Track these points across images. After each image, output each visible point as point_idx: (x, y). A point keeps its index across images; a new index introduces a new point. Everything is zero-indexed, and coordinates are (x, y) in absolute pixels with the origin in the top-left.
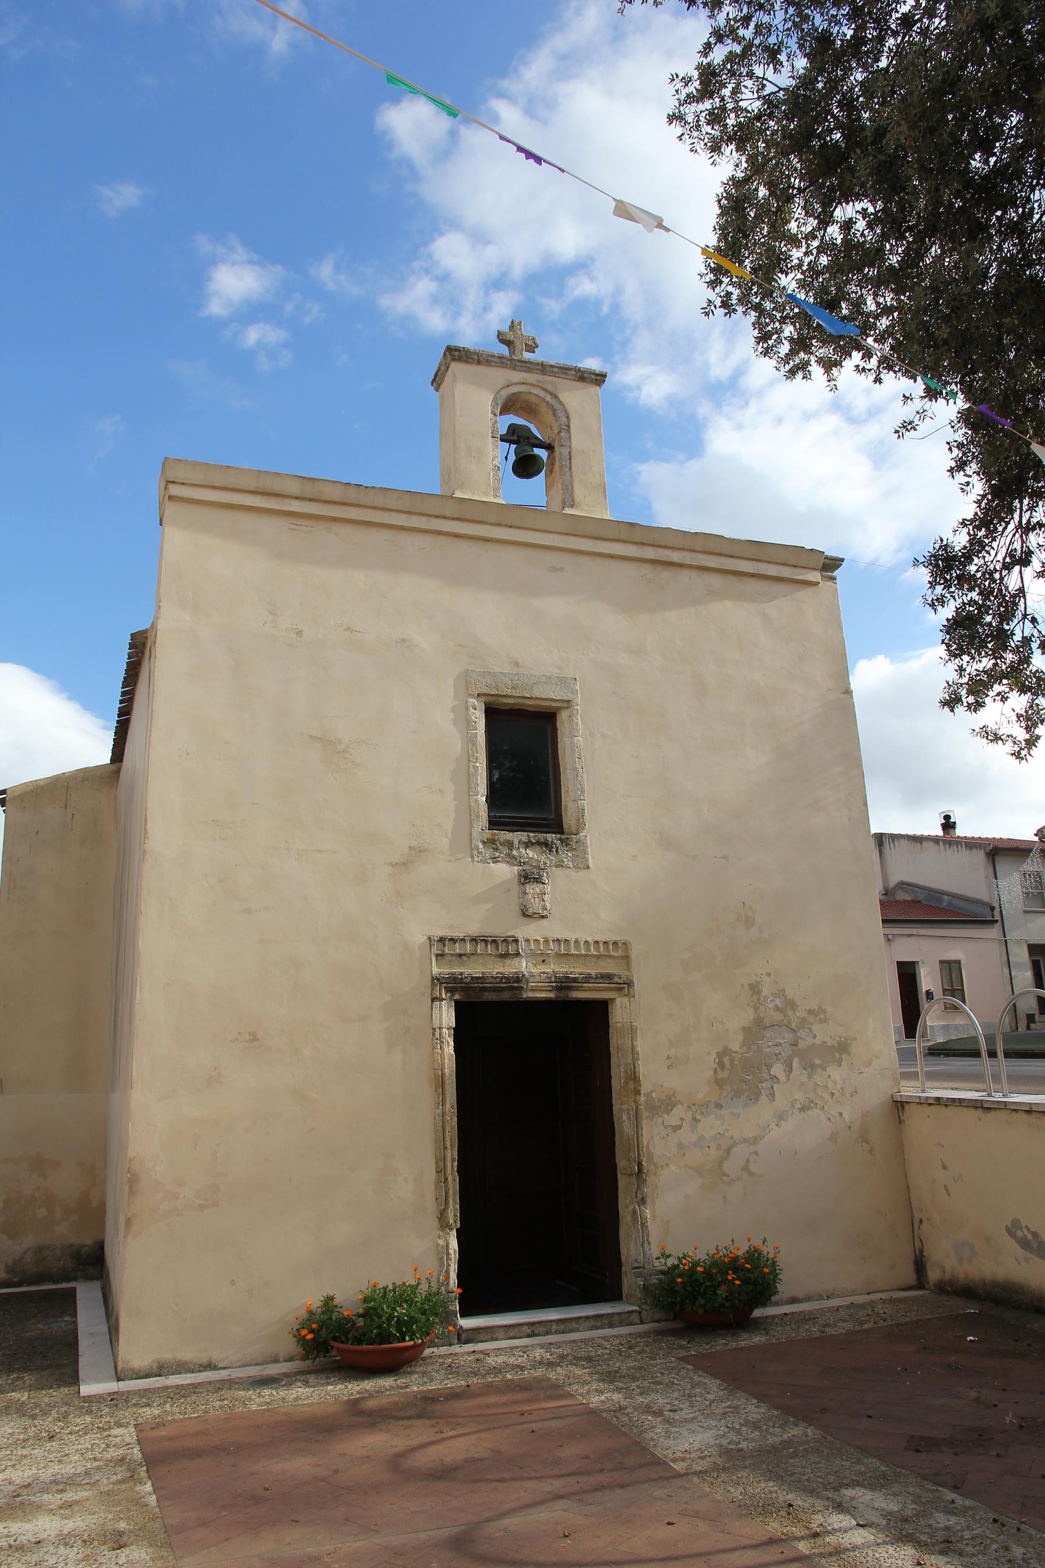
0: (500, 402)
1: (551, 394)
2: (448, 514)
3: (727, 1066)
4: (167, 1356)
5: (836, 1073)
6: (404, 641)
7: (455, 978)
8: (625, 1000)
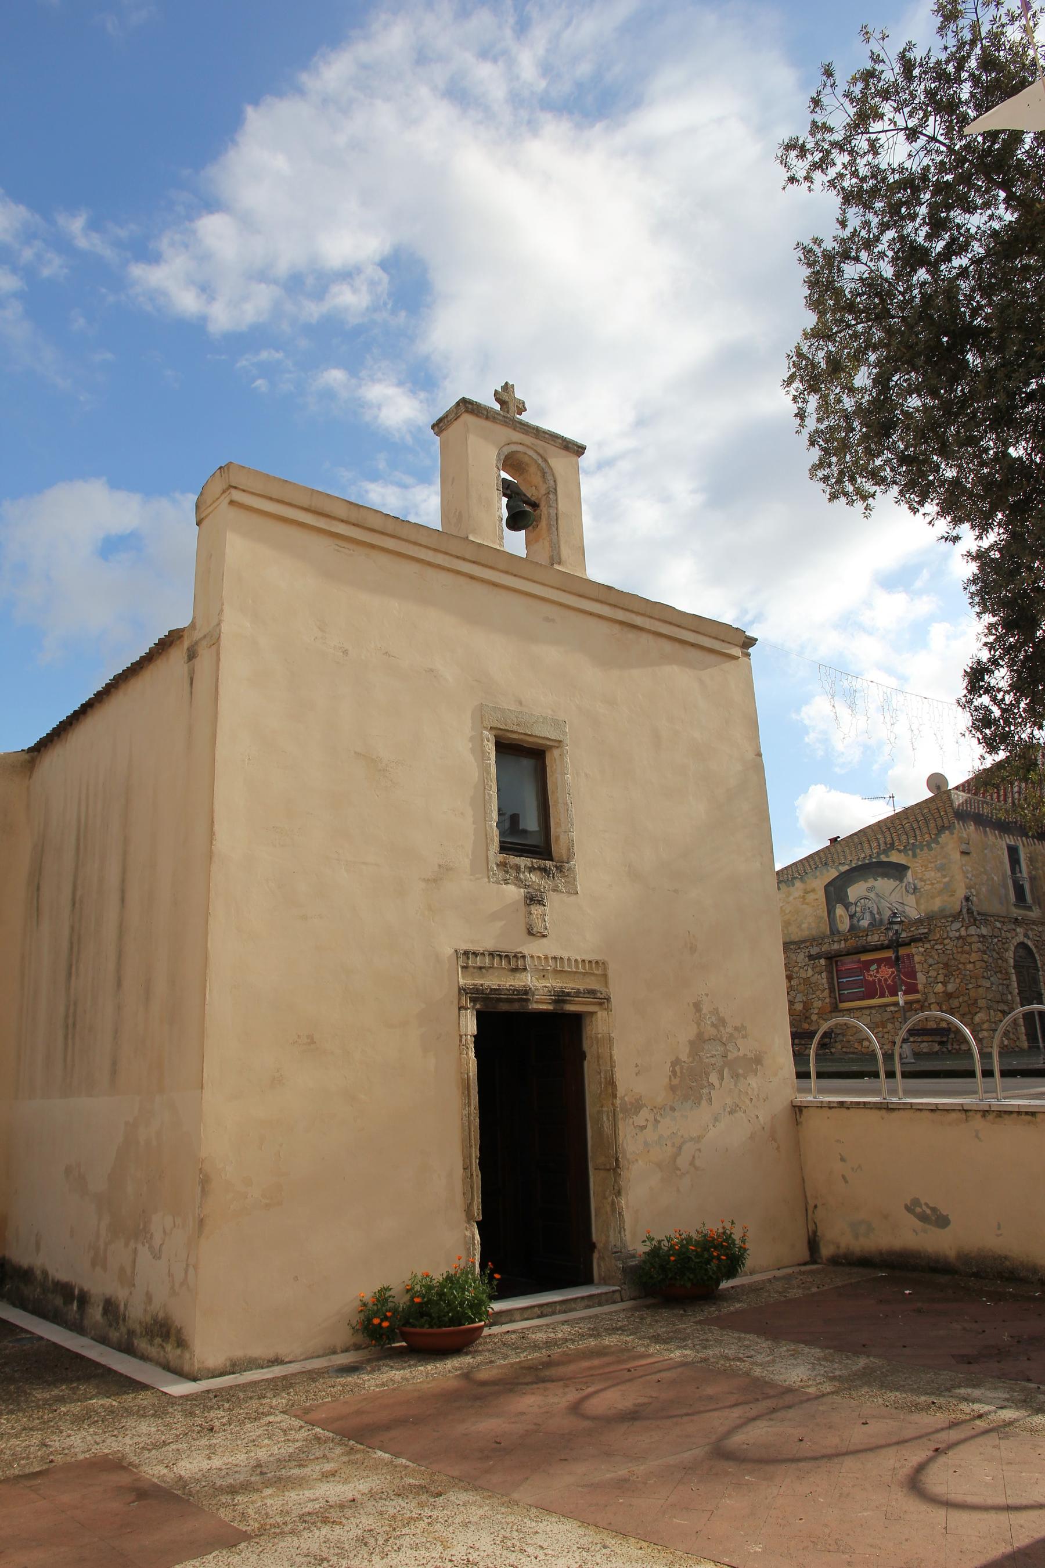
0: (503, 457)
1: (542, 457)
2: (467, 556)
3: (679, 1074)
4: (239, 1353)
5: (753, 1082)
6: (432, 670)
7: (477, 989)
8: (605, 1013)
